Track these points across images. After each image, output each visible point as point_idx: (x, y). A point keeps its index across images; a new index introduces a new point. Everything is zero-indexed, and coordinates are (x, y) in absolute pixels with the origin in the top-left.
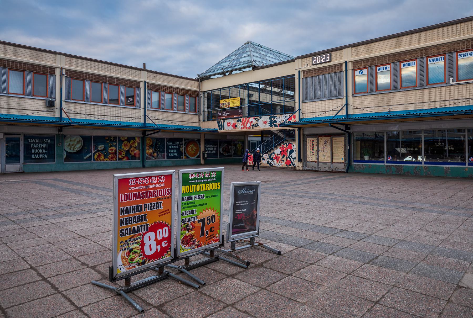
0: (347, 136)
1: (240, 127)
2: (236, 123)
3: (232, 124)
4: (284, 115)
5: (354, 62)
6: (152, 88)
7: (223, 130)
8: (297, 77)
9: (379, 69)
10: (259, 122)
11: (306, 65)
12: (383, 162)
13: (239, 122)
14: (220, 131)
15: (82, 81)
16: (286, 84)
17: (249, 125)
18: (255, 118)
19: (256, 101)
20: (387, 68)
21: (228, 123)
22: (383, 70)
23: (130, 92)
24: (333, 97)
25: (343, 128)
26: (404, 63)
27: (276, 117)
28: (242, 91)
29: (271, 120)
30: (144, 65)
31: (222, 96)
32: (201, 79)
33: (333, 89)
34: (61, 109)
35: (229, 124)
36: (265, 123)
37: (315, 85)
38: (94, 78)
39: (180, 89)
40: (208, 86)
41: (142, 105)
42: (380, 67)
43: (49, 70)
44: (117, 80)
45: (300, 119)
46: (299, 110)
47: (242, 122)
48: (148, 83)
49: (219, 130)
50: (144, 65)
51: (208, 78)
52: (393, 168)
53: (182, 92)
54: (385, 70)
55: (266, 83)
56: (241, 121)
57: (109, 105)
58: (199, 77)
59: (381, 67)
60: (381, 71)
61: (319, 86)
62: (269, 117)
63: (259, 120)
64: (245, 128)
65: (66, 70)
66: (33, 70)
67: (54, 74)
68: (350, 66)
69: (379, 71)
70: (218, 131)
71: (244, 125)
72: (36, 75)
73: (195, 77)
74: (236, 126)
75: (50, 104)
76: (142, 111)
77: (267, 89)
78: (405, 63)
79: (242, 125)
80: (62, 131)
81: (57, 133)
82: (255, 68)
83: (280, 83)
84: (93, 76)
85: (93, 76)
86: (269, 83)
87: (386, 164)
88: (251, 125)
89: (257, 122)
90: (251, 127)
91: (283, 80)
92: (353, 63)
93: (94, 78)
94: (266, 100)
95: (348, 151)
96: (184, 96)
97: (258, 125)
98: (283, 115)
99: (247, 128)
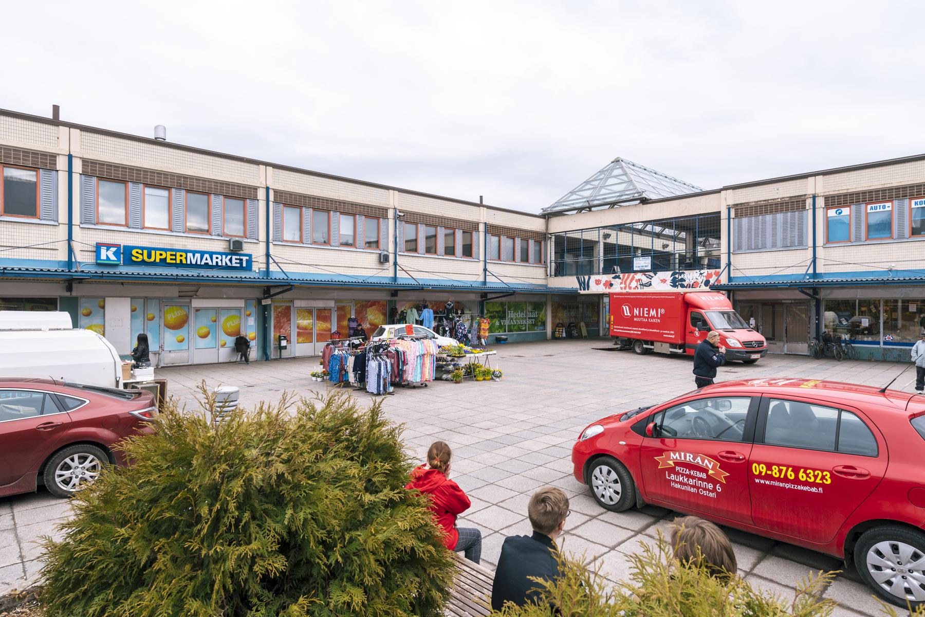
0: (815, 303)
1: (619, 286)
2: (610, 281)
3: (603, 281)
4: (698, 271)
5: (827, 198)
6: (492, 230)
7: (588, 290)
8: (724, 215)
9: (872, 208)
10: (652, 280)
11: (733, 198)
12: (878, 343)
13: (617, 279)
14: (582, 292)
15: (352, 217)
16: (701, 225)
17: (634, 284)
18: (645, 275)
19: (647, 249)
20: (886, 206)
21: (596, 280)
22: (878, 210)
23: (431, 231)
24: (788, 247)
25: (810, 292)
26: (916, 201)
27: (684, 273)
28: (655, 240)
29: (675, 278)
30: (481, 197)
31: (584, 240)
32: (547, 216)
33: (789, 236)
34: (395, 264)
35: (598, 282)
36: (664, 281)
37: (757, 229)
38: (214, 188)
39: (372, 207)
40: (558, 226)
41: (482, 257)
42: (873, 206)
43: (107, 169)
44: (229, 188)
45: (730, 279)
46: (729, 264)
47: (622, 280)
48: (276, 191)
49: (581, 290)
50: (481, 197)
51: (560, 214)
52: (427, 325)
53: (526, 235)
54: (882, 210)
55: (665, 223)
56: (620, 278)
57: (445, 257)
58: (544, 211)
59: (876, 205)
60: (874, 211)
61: (764, 231)
62: (670, 273)
63: (652, 277)
64: (627, 288)
65: (83, 161)
66: (187, 187)
67: (386, 217)
68: (820, 202)
69: (872, 211)
70: (579, 291)
71: (625, 284)
72: (189, 195)
73: (539, 212)
74: (611, 285)
75: (383, 259)
76: (482, 264)
77: (664, 233)
78: (919, 200)
79: (621, 283)
80: (397, 296)
81: (389, 298)
82: (644, 201)
83: (690, 224)
84: (193, 182)
85: (223, 187)
86: (670, 223)
87: (882, 346)
88: (639, 283)
89: (649, 280)
90: (639, 286)
91: (696, 219)
92: (825, 198)
93: (214, 188)
94: (645, 245)
95: (815, 326)
96: (514, 239)
97: (650, 285)
98: (695, 271)
99: (630, 288)
